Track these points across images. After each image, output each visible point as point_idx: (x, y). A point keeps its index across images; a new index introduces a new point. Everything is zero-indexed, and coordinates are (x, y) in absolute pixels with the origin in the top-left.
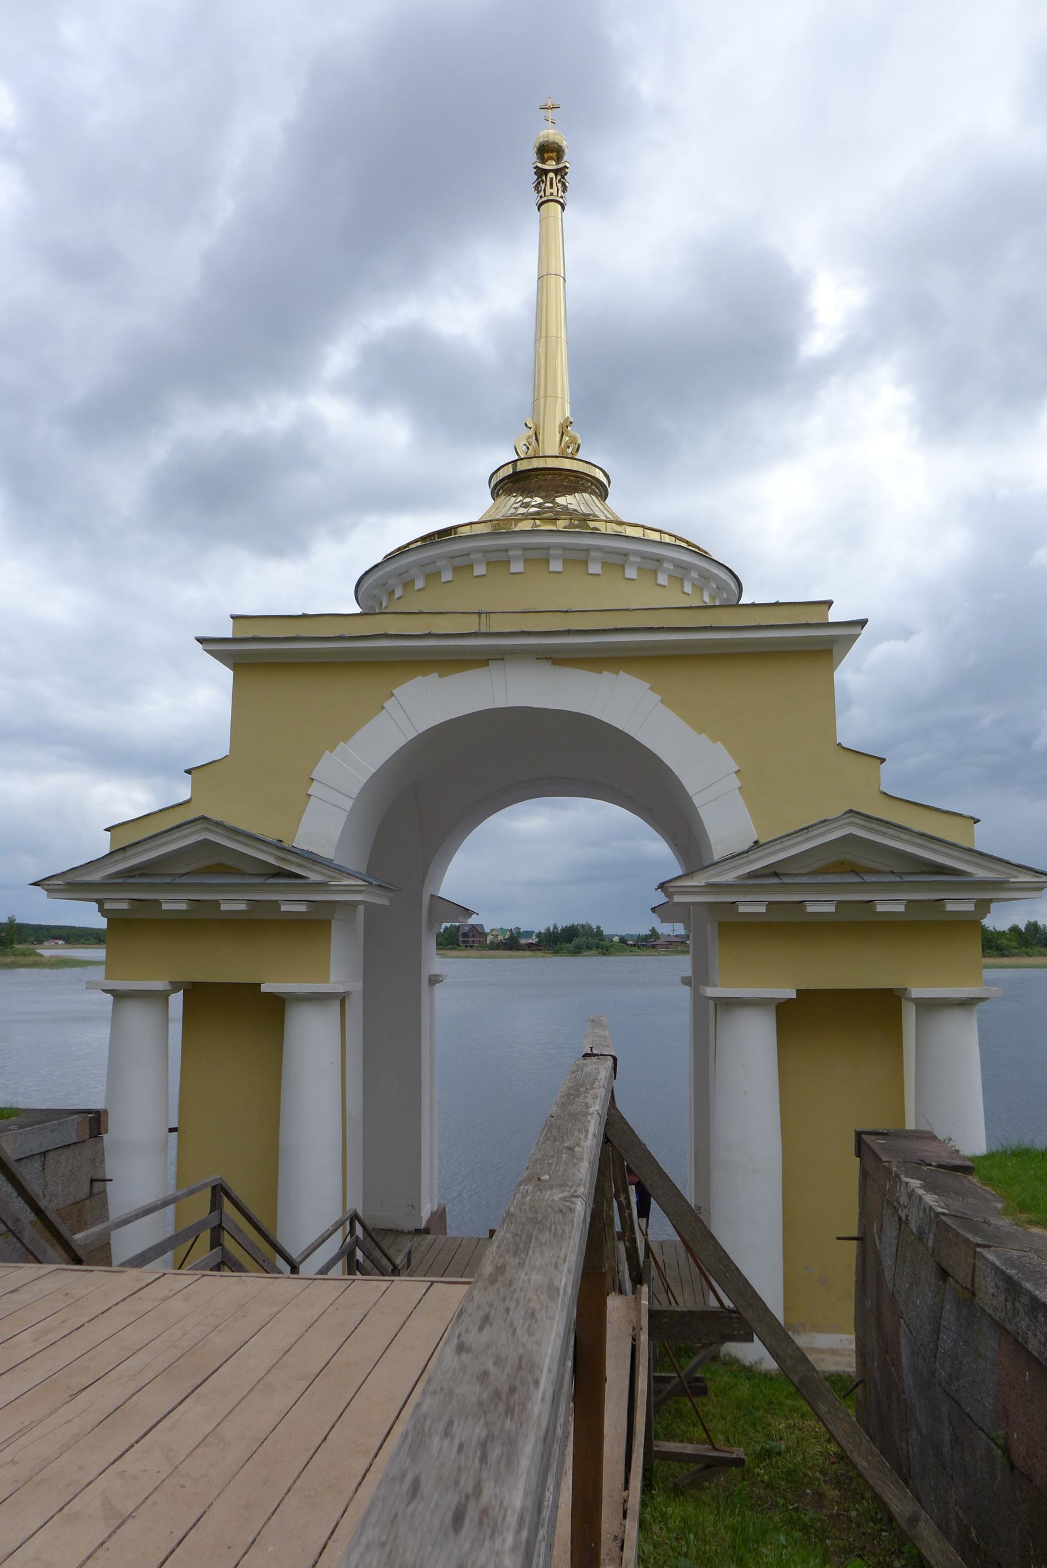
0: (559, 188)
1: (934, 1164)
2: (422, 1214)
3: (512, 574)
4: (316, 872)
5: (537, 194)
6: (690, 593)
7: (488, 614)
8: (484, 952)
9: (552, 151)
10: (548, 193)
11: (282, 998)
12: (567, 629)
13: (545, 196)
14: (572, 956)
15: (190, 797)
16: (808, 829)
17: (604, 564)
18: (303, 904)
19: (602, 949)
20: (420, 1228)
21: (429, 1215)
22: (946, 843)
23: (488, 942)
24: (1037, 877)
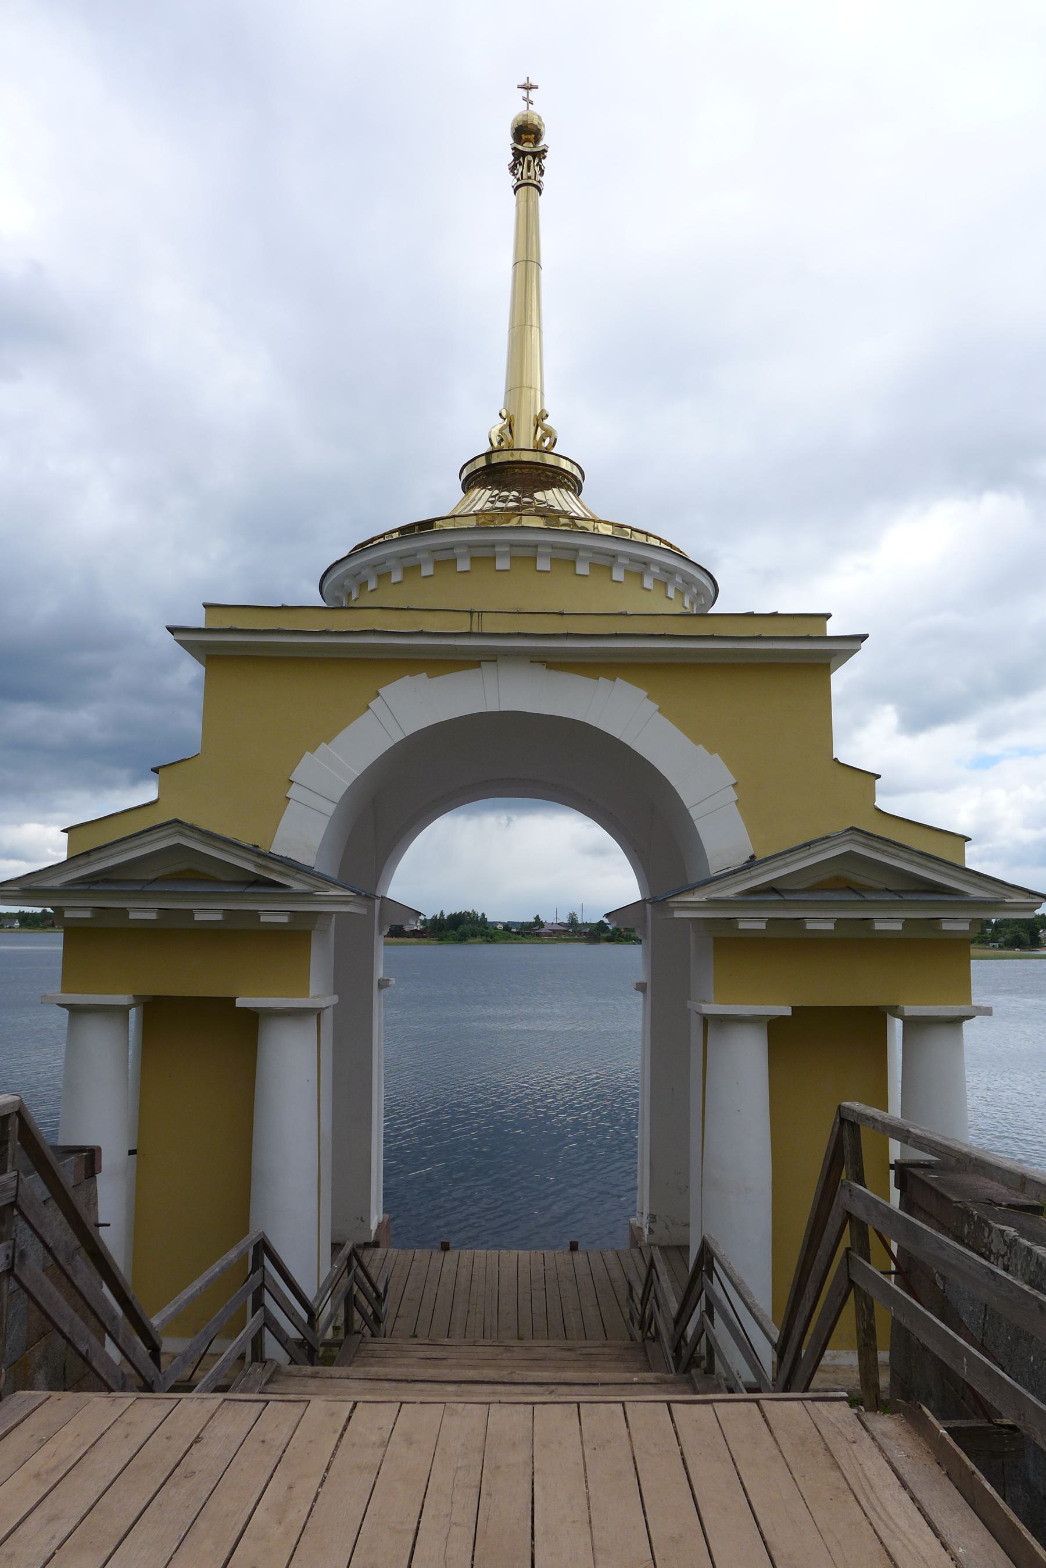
0: (537, 172)
1: (1004, 1203)
4: (300, 880)
5: (514, 177)
6: (673, 597)
7: (480, 613)
9: (530, 133)
10: (525, 177)
11: (255, 1012)
12: (566, 632)
14: (457, 943)
15: (157, 798)
17: (592, 565)
18: (284, 915)
19: (487, 936)
22: (947, 863)
24: (1030, 898)
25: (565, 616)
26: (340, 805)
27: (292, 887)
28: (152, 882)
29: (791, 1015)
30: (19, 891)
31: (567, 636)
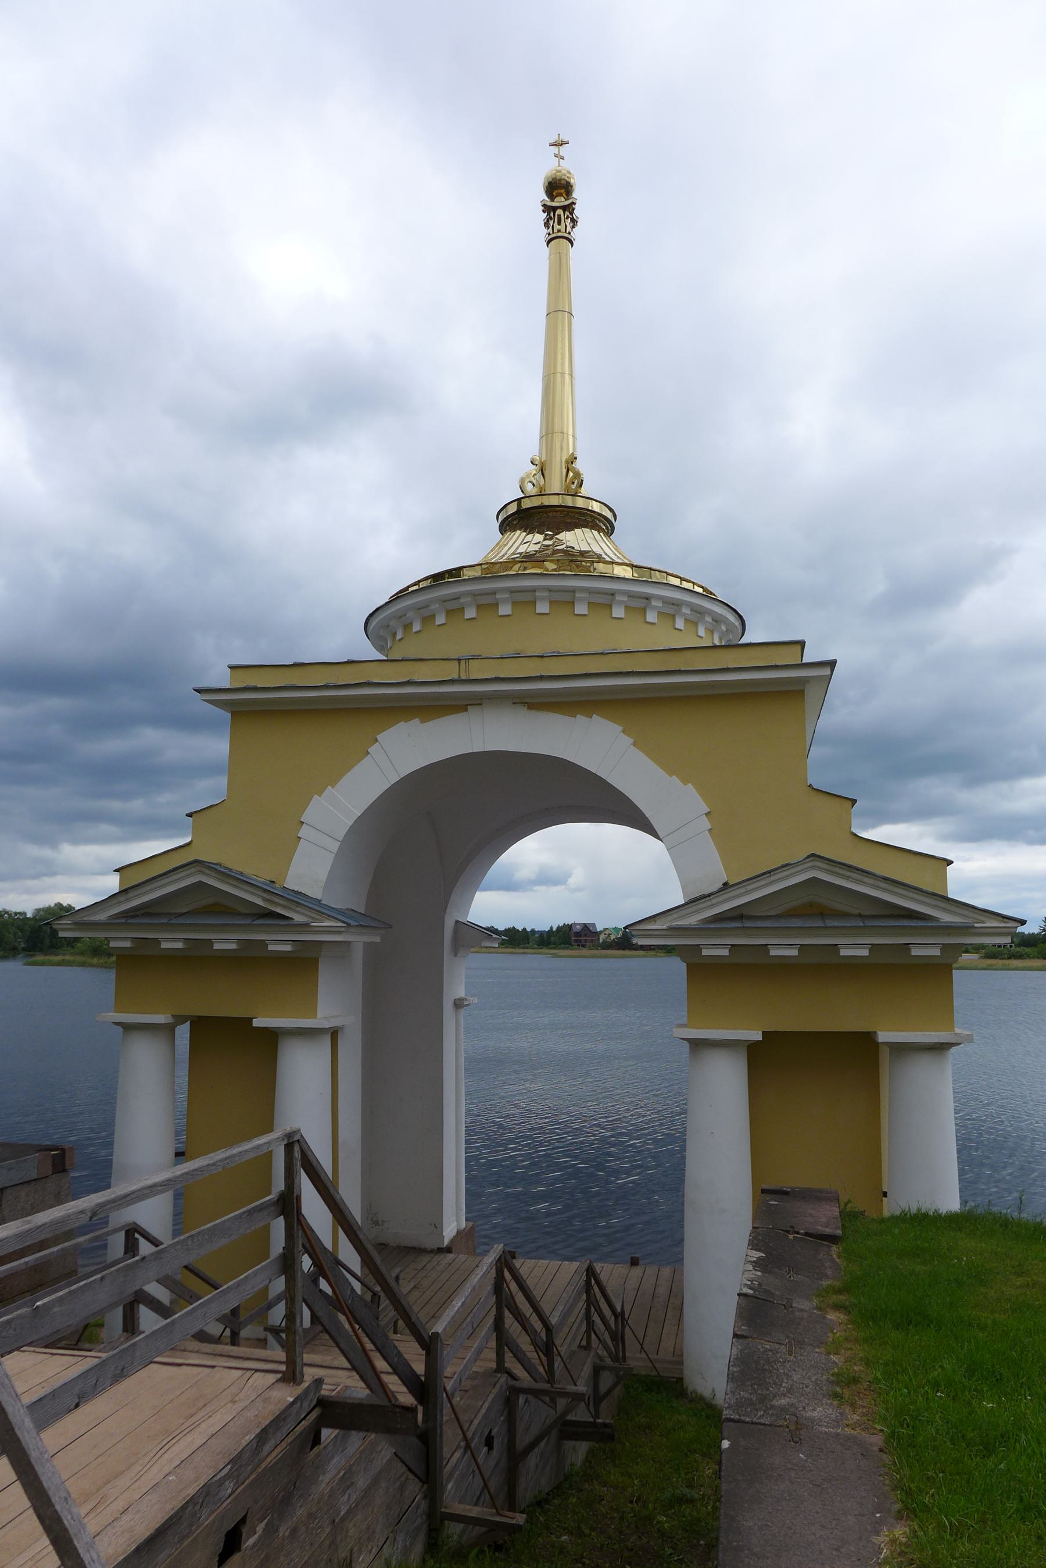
2: (444, 1234)
3: (500, 616)
7: (467, 660)
8: (596, 952)
9: (562, 187)
10: (555, 231)
13: (553, 232)
16: (770, 873)
17: (591, 605)
18: (289, 944)
20: (442, 1247)
21: (454, 1233)
23: (601, 941)
25: (544, 658)
26: (344, 842)
27: (293, 919)
28: (180, 916)
29: (761, 1039)
30: (72, 924)
31: (541, 678)
